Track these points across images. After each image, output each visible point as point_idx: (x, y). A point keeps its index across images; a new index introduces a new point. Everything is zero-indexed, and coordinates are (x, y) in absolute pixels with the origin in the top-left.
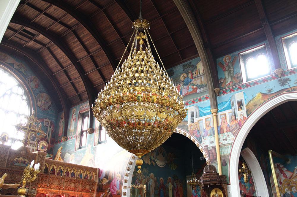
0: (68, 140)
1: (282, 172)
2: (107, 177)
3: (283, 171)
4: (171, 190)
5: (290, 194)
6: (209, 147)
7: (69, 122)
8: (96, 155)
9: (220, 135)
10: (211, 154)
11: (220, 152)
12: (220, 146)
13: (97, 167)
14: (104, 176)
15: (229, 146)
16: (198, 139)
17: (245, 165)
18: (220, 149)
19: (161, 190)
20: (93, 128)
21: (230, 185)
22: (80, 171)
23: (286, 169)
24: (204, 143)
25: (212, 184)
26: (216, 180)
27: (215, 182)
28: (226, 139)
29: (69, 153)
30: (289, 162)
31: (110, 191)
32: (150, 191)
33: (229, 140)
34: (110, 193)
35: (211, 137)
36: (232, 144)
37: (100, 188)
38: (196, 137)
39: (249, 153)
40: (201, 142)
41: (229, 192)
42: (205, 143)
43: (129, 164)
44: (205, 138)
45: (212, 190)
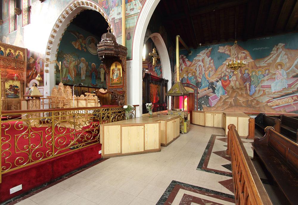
0: (4, 23)
1: (184, 61)
2: (33, 56)
3: (185, 61)
4: (103, 74)
5: (186, 78)
6: (115, 19)
7: (3, 5)
8: (24, 36)
9: (128, 4)
10: (117, 27)
11: (125, 24)
12: (127, 17)
13: (25, 47)
14: (31, 55)
15: (135, 17)
16: (106, 12)
17: (155, 50)
18: (126, 20)
19: (93, 73)
20: (21, 9)
21: (132, 61)
22: (10, 50)
23: (187, 60)
24: (111, 16)
25: (107, 53)
26: (112, 50)
27: (111, 52)
28: (133, 9)
29: (5, 36)
30: (190, 54)
31: (35, 69)
32: (81, 72)
33: (135, 9)
34: (36, 70)
35: (119, 7)
36: (138, 14)
37: (28, 67)
38: (105, 8)
39: (161, 44)
40: (109, 14)
41: (131, 67)
42: (112, 15)
43: (49, 43)
44: (112, 9)
45: (112, 63)
